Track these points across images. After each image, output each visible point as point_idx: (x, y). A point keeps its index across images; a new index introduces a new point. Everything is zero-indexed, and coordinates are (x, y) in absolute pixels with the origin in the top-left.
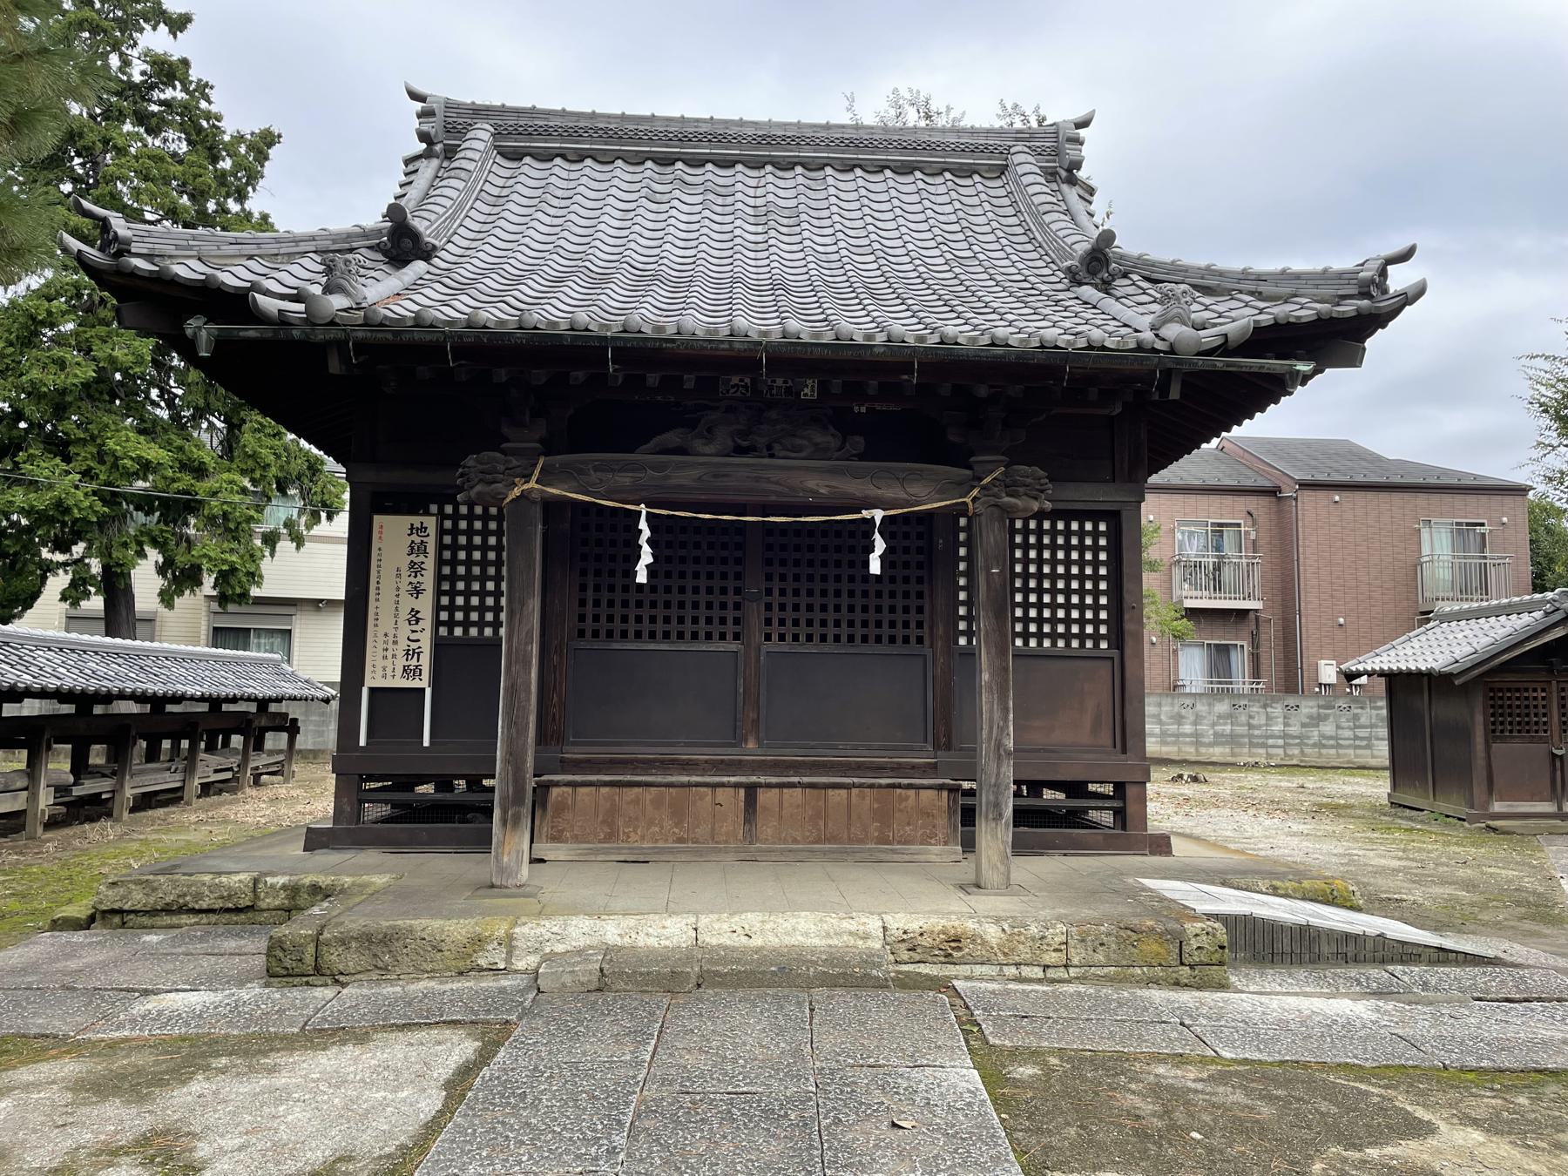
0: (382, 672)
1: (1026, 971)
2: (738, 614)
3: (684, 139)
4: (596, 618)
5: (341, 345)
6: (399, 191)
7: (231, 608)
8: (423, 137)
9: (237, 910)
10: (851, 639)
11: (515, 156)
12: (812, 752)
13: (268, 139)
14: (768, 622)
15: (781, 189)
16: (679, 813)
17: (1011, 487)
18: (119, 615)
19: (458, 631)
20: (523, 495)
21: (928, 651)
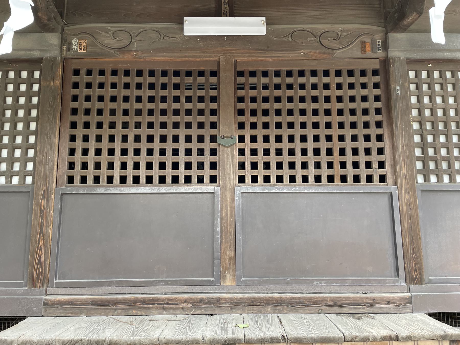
2: (213, 159)
4: (124, 166)
10: (318, 179)
12: (288, 288)
14: (242, 166)
19: (16, 180)
21: (394, 189)
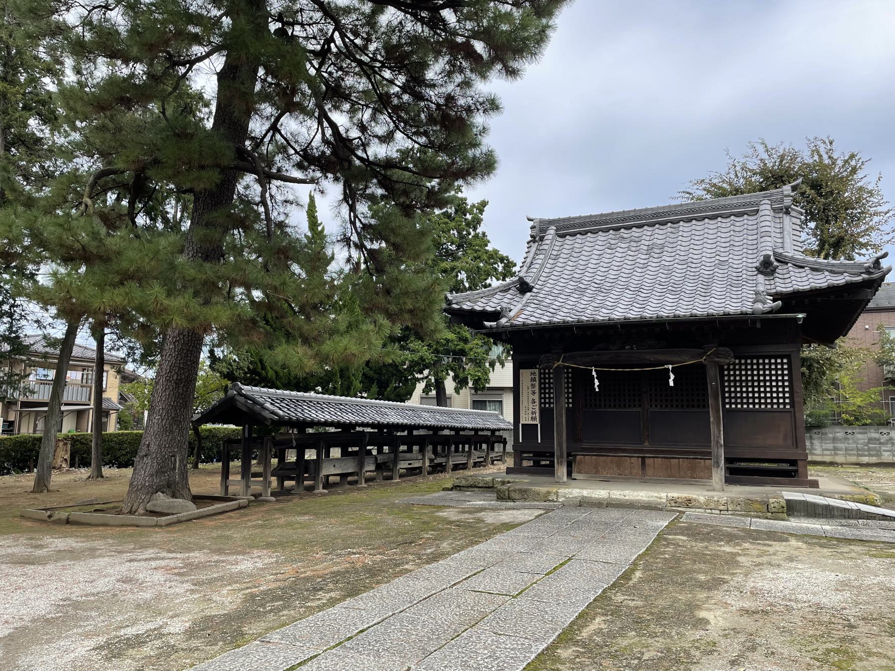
0: (525, 419)
1: (714, 511)
3: (624, 220)
5: (505, 332)
6: (525, 255)
7: (479, 392)
8: (532, 236)
9: (489, 487)
11: (563, 236)
13: (484, 204)
14: (651, 401)
15: (659, 234)
16: (619, 466)
17: (717, 354)
18: (442, 399)
20: (558, 366)
